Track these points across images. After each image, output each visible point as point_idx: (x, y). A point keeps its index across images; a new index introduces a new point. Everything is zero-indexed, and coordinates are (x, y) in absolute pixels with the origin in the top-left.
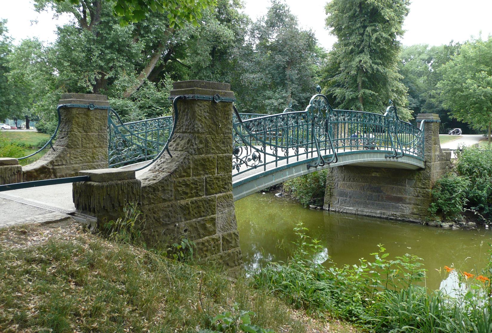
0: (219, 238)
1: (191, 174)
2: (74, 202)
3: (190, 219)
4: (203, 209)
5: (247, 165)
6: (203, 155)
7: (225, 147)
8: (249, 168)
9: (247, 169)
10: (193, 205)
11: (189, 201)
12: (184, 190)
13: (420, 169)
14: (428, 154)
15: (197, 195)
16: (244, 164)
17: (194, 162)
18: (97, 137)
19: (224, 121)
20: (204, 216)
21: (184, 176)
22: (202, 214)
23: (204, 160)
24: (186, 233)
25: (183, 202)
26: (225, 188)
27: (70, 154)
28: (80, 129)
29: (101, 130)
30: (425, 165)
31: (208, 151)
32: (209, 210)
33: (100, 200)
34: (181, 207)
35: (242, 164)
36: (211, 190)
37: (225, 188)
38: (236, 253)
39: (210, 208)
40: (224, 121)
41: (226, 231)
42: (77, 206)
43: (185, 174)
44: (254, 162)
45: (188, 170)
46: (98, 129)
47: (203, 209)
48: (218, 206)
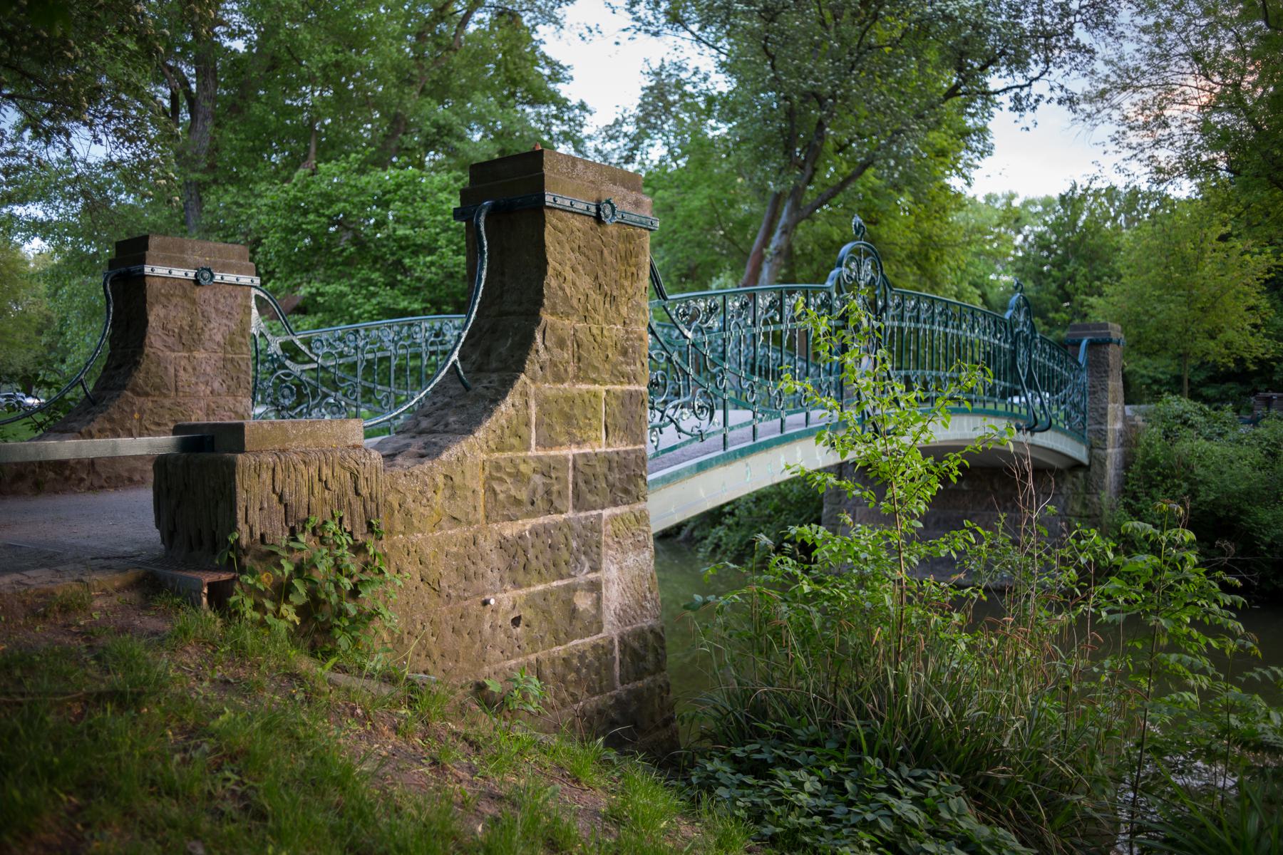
0: (612, 641)
1: (533, 442)
2: (157, 527)
3: (529, 585)
4: (565, 555)
5: (679, 430)
6: (566, 385)
7: (628, 364)
8: (685, 437)
9: (679, 441)
10: (538, 542)
11: (526, 525)
12: (513, 492)
13: (1076, 466)
14: (1097, 427)
15: (552, 508)
16: (673, 425)
17: (540, 405)
18: (220, 364)
19: (627, 283)
20: (570, 576)
21: (512, 448)
22: (564, 570)
23: (571, 400)
24: (519, 629)
25: (510, 530)
26: (626, 491)
27: (142, 412)
28: (170, 341)
29: (232, 345)
30: (1090, 456)
31: (581, 374)
32: (583, 557)
33: (250, 512)
34: (502, 545)
35: (665, 425)
36: (589, 496)
37: (626, 491)
38: (657, 690)
39: (585, 553)
40: (627, 283)
41: (631, 624)
42: (169, 535)
43: (515, 441)
44: (697, 422)
45: (523, 430)
46: (222, 342)
47: (565, 555)
48: (608, 545)
